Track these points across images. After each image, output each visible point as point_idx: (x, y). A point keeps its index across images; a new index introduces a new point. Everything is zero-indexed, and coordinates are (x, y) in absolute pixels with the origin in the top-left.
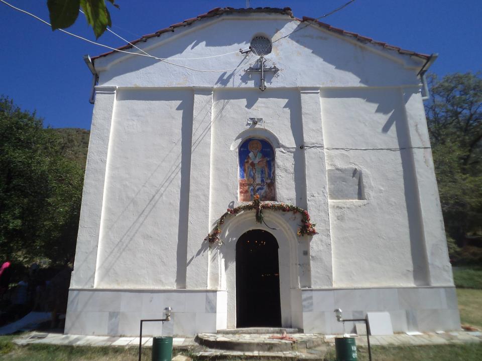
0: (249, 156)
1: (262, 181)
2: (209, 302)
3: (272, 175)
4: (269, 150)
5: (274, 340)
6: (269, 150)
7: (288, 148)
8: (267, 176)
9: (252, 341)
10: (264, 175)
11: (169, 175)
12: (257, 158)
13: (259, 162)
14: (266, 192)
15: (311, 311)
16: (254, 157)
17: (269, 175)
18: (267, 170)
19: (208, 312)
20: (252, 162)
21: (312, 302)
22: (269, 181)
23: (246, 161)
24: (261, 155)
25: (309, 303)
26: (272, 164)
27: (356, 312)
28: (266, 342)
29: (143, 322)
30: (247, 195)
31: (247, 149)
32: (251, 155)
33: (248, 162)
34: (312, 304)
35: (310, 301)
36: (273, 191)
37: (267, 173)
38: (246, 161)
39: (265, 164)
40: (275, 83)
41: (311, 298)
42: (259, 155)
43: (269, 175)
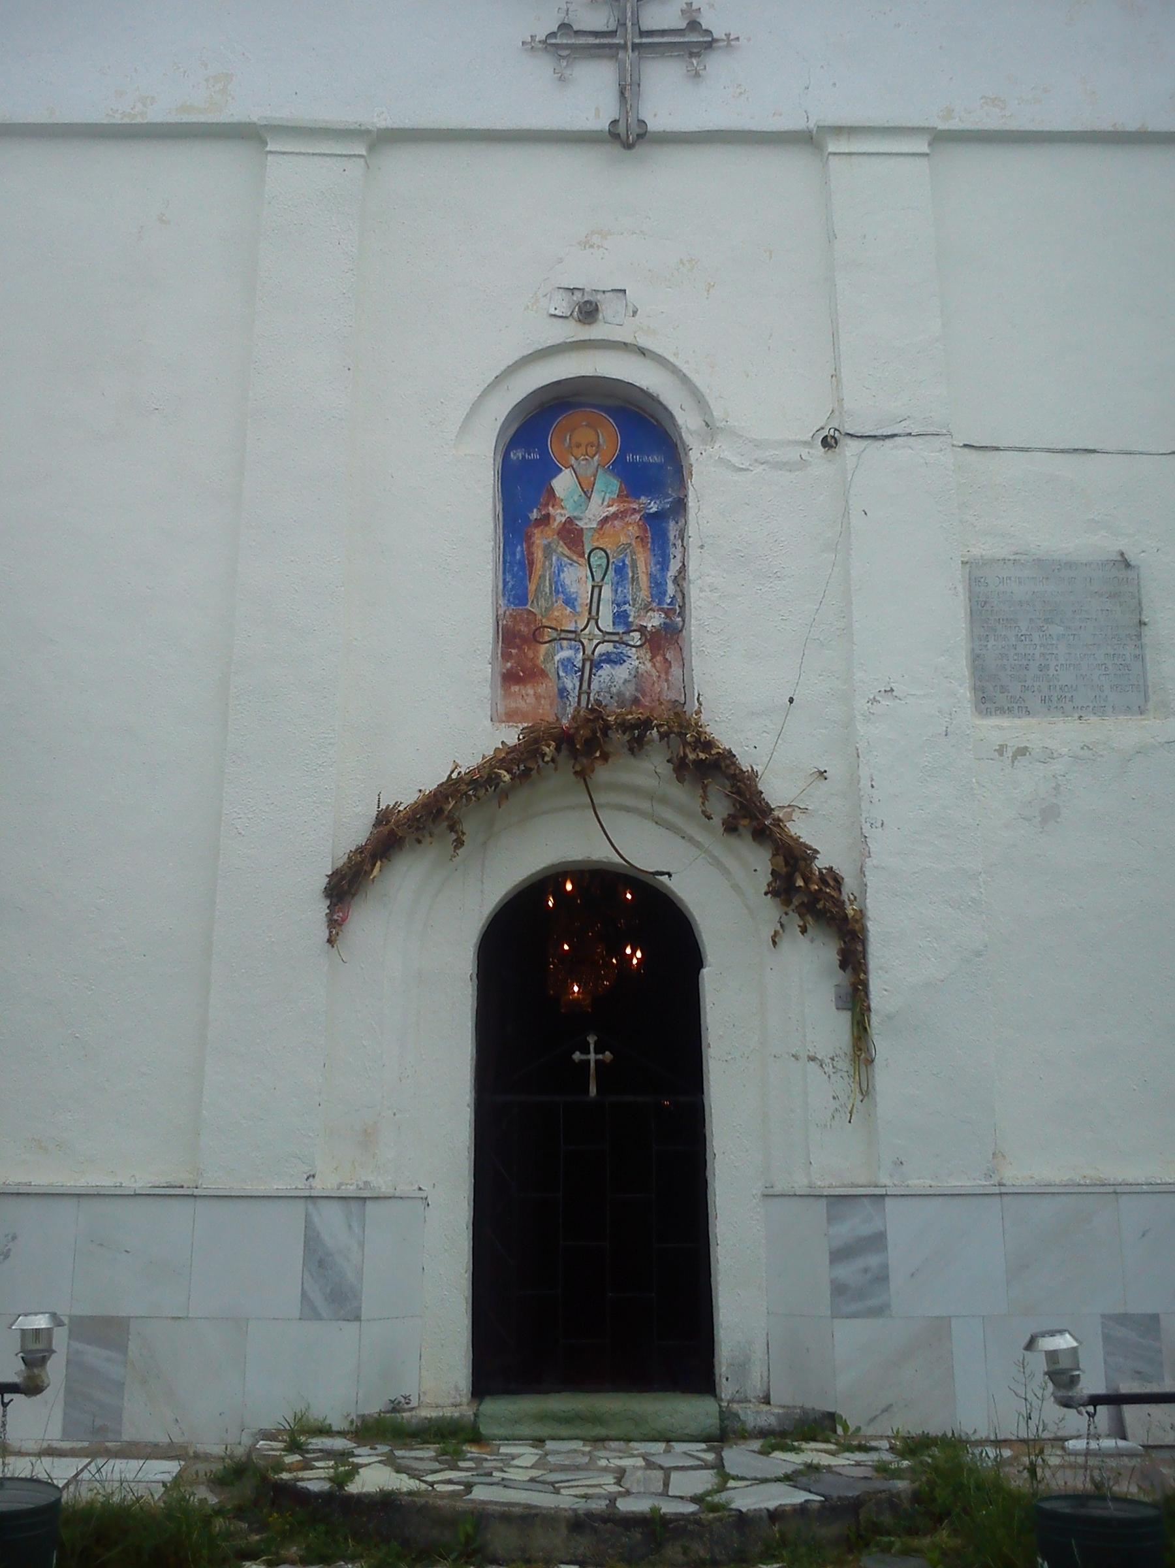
0: (551, 491)
1: (620, 617)
2: (321, 1264)
3: (671, 589)
4: (655, 459)
5: (679, 1447)
6: (655, 459)
7: (758, 444)
8: (644, 594)
9: (543, 1500)
10: (629, 590)
11: (592, 40)
12: (596, 498)
13: (605, 520)
14: (637, 675)
15: (879, 1311)
16: (583, 492)
17: (658, 586)
18: (643, 563)
19: (318, 1317)
20: (570, 521)
21: (885, 1267)
22: (654, 620)
23: (535, 515)
24: (615, 484)
25: (866, 1270)
26: (672, 529)
27: (1123, 1319)
28: (625, 1506)
29: (644, 28)
30: (541, 689)
31: (544, 452)
32: (563, 483)
33: (546, 519)
34: (882, 1278)
35: (873, 1261)
36: (676, 670)
37: (644, 580)
38: (535, 515)
39: (633, 530)
40: (634, 628)
41: (877, 1241)
42: (607, 488)
43: (658, 586)
